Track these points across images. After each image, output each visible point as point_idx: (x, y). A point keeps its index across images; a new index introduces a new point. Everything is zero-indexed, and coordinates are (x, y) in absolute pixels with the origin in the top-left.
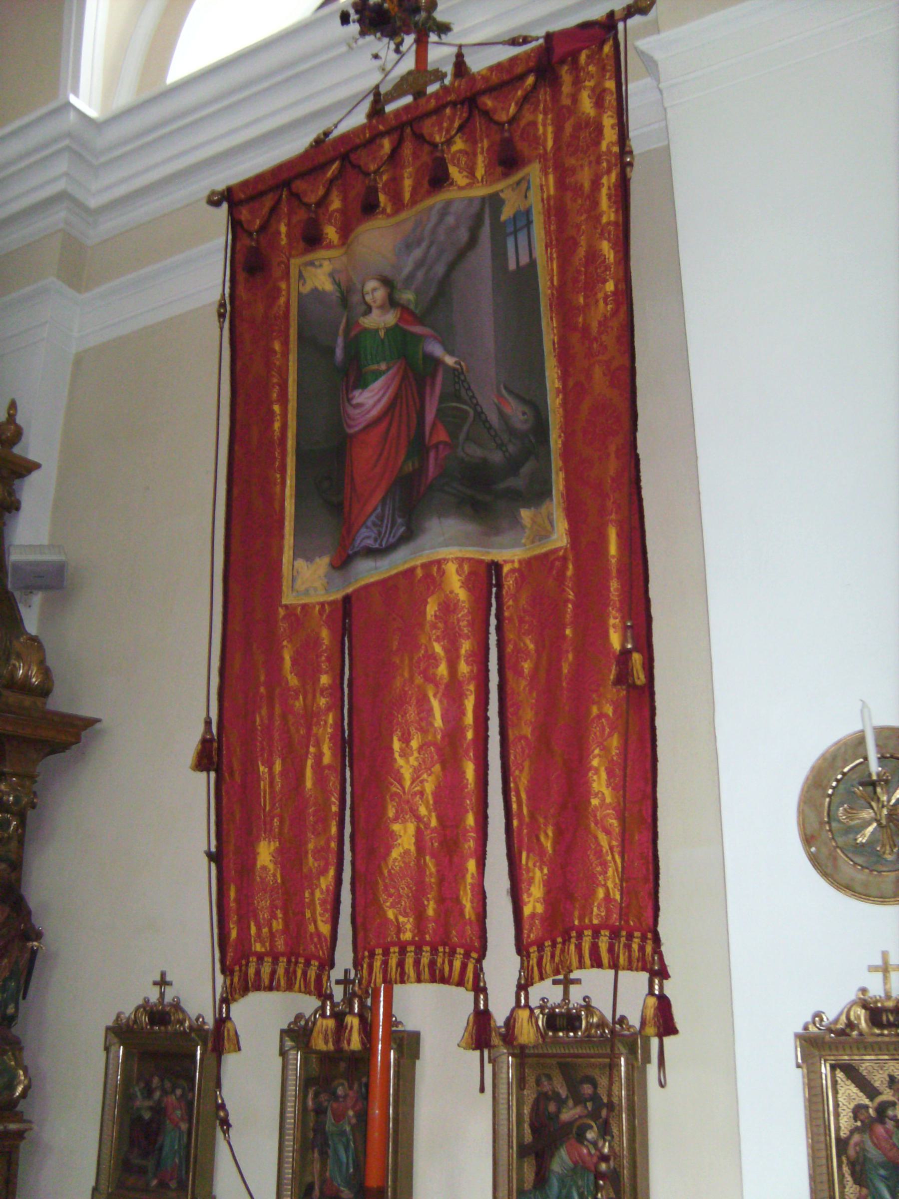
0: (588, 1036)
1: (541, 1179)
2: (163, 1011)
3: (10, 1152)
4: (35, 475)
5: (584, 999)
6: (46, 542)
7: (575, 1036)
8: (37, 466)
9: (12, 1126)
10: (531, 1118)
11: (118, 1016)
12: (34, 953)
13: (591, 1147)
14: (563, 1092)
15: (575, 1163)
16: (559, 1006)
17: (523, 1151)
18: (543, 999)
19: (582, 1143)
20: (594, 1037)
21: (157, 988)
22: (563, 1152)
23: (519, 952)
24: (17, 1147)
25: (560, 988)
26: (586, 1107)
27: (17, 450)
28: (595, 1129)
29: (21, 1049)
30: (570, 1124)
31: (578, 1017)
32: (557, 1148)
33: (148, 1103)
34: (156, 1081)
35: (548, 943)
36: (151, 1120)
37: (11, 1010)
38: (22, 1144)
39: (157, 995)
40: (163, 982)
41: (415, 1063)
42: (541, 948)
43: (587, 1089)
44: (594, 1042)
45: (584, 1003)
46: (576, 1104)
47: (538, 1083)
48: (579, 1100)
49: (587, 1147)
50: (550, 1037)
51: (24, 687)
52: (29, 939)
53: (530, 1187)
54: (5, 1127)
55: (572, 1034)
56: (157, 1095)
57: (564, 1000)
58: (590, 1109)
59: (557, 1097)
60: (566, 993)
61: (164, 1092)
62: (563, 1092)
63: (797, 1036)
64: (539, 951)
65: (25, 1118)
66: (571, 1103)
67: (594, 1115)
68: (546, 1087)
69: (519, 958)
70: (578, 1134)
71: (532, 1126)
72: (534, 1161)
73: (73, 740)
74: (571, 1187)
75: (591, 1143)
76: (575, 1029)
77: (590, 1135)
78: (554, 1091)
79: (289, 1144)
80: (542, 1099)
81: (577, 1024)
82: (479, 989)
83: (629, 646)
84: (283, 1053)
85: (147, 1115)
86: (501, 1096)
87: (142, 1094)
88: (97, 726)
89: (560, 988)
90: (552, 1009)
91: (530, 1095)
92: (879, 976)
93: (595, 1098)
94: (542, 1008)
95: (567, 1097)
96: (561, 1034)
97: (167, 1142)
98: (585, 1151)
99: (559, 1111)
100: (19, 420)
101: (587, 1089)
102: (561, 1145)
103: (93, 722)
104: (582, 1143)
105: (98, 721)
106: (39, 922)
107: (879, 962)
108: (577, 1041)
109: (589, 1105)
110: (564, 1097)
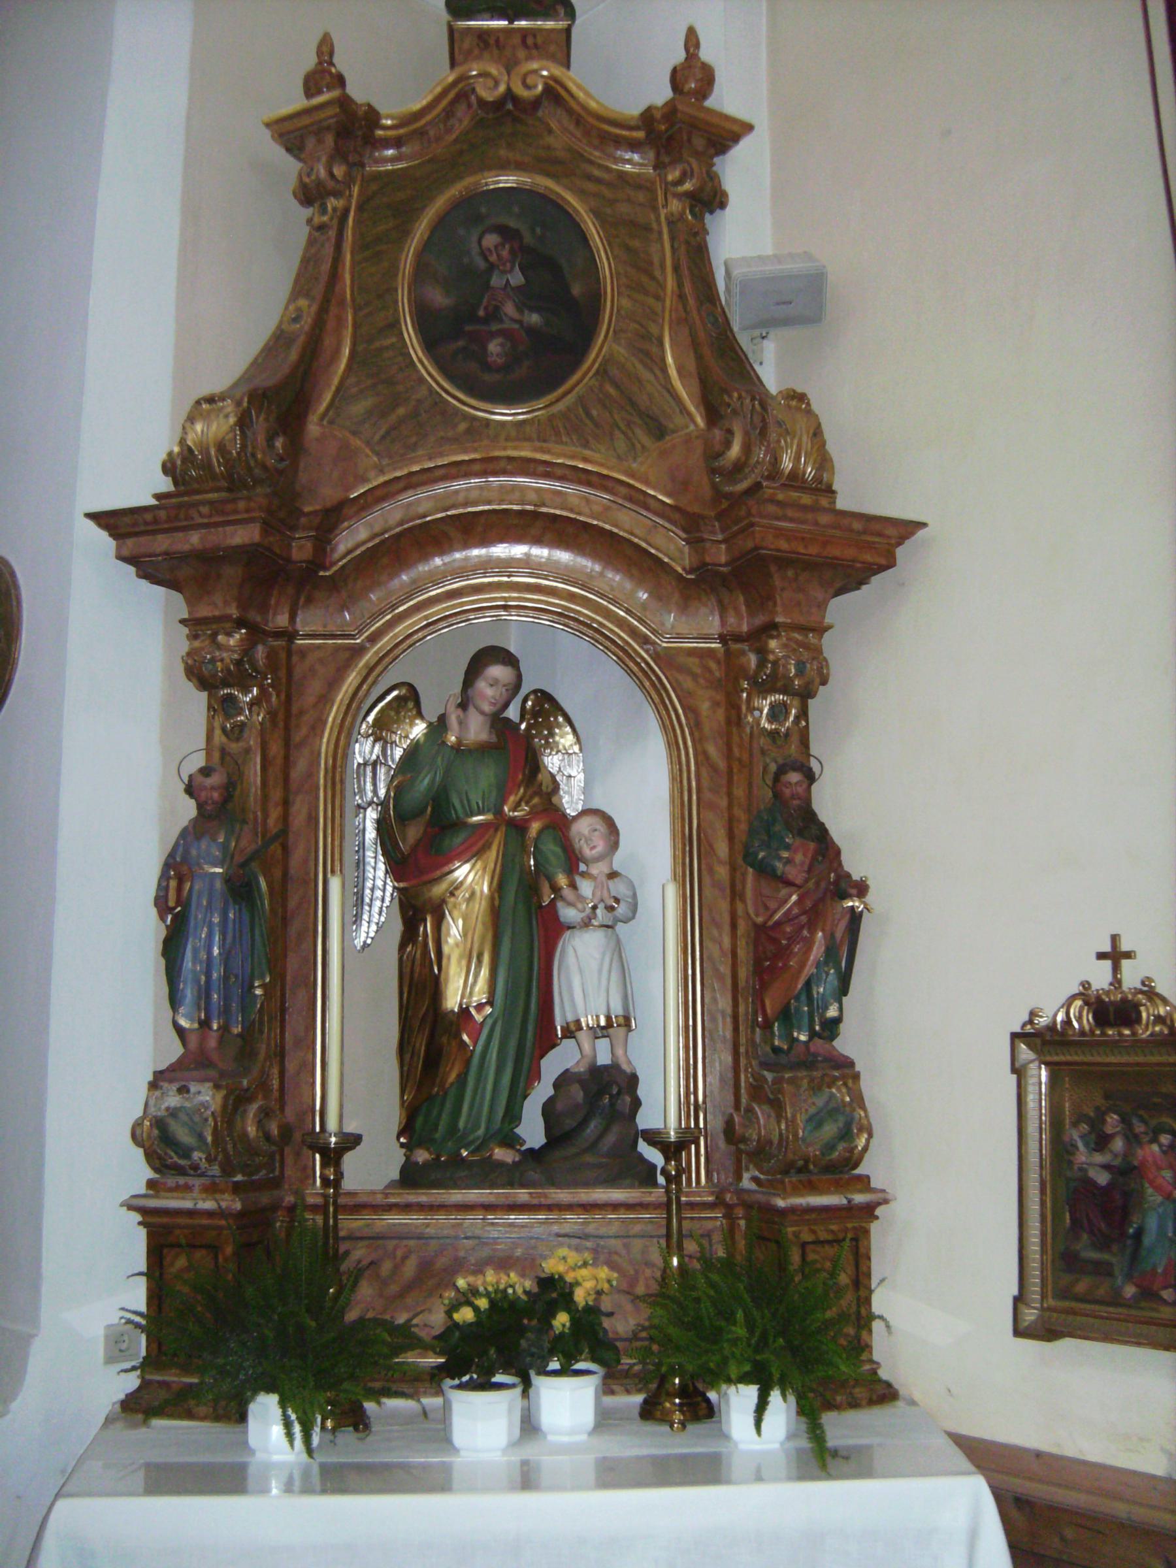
2: (1124, 1000)
3: (855, 1240)
4: (745, 144)
6: (770, 252)
8: (749, 128)
9: (859, 1198)
11: (1033, 1014)
12: (855, 919)
21: (1107, 964)
24: (867, 1232)
27: (709, 103)
29: (856, 1077)
33: (1099, 1158)
34: (1112, 1119)
36: (1111, 1186)
37: (832, 1012)
38: (874, 1227)
39: (1108, 977)
40: (1115, 956)
51: (795, 480)
52: (845, 896)
54: (849, 1201)
56: (1118, 1144)
61: (1132, 1139)
63: (1039, 1039)
65: (873, 1185)
73: (883, 562)
79: (1034, 1207)
84: (1018, 1070)
85: (1103, 1178)
87: (1086, 1145)
88: (921, 534)
92: (1107, 964)
97: (1152, 1223)
100: (706, 54)
103: (908, 529)
105: (924, 525)
106: (855, 865)
107: (1125, 946)
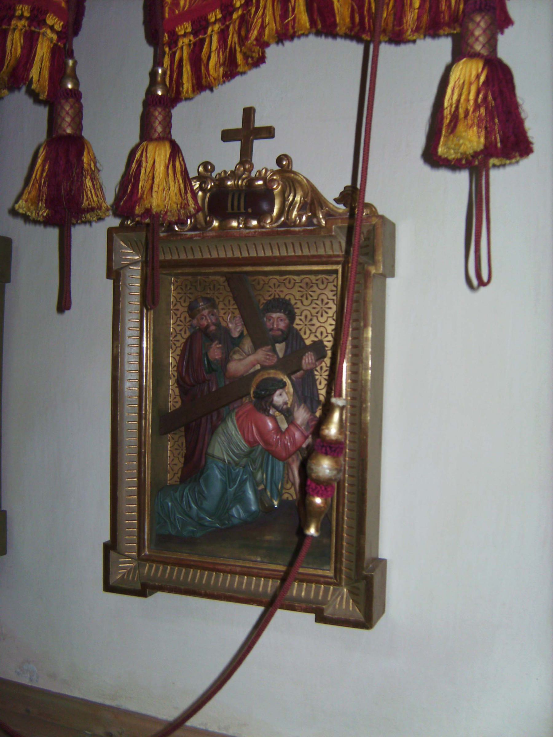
0: (284, 224)
1: (195, 464)
5: (279, 161)
7: (260, 226)
10: (179, 371)
13: (281, 418)
14: (236, 328)
15: (252, 444)
16: (234, 175)
17: (165, 422)
18: (205, 164)
19: (266, 411)
20: (295, 225)
22: (231, 427)
23: (153, 36)
25: (236, 146)
26: (274, 350)
28: (290, 388)
30: (247, 379)
31: (267, 194)
32: (222, 419)
35: (215, 15)
41: (4, 287)
42: (200, 27)
43: (277, 320)
44: (294, 233)
45: (277, 168)
46: (256, 346)
47: (192, 311)
48: (261, 338)
49: (274, 418)
50: (214, 229)
53: (176, 478)
55: (254, 223)
57: (242, 162)
58: (281, 355)
59: (223, 336)
60: (246, 155)
62: (236, 328)
64: (195, 33)
66: (247, 344)
67: (290, 364)
68: (206, 319)
69: (150, 51)
70: (257, 396)
71: (180, 382)
72: (183, 440)
74: (243, 483)
75: (281, 411)
76: (260, 215)
77: (280, 398)
78: (218, 325)
80: (198, 338)
81: (265, 206)
82: (61, 97)
83: (241, 226)
86: (128, 333)
89: (236, 146)
90: (221, 180)
91: (177, 328)
93: (291, 336)
94: (201, 178)
95: (241, 335)
96: (235, 224)
98: (270, 425)
99: (226, 359)
101: (277, 320)
102: (229, 414)
104: (266, 411)
108: (262, 234)
109: (280, 348)
110: (236, 335)
